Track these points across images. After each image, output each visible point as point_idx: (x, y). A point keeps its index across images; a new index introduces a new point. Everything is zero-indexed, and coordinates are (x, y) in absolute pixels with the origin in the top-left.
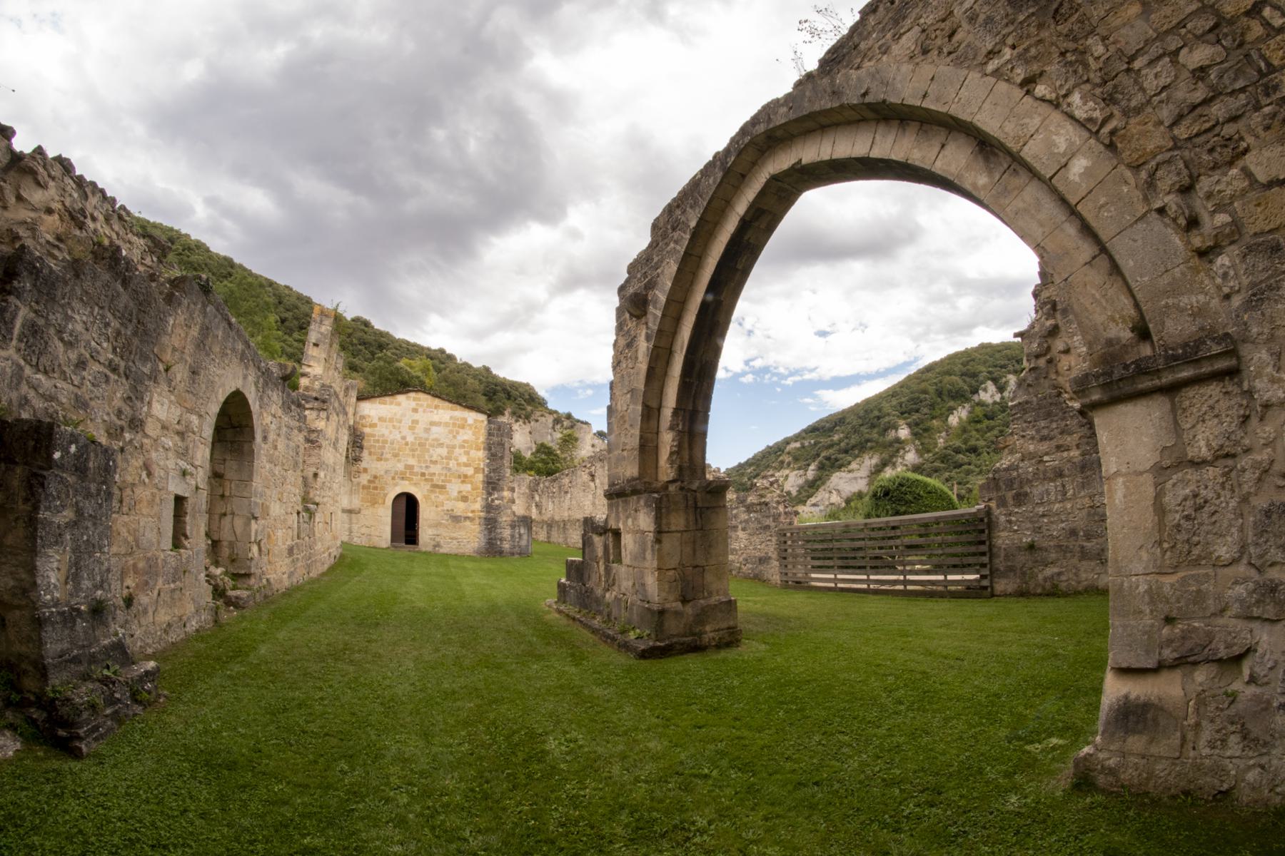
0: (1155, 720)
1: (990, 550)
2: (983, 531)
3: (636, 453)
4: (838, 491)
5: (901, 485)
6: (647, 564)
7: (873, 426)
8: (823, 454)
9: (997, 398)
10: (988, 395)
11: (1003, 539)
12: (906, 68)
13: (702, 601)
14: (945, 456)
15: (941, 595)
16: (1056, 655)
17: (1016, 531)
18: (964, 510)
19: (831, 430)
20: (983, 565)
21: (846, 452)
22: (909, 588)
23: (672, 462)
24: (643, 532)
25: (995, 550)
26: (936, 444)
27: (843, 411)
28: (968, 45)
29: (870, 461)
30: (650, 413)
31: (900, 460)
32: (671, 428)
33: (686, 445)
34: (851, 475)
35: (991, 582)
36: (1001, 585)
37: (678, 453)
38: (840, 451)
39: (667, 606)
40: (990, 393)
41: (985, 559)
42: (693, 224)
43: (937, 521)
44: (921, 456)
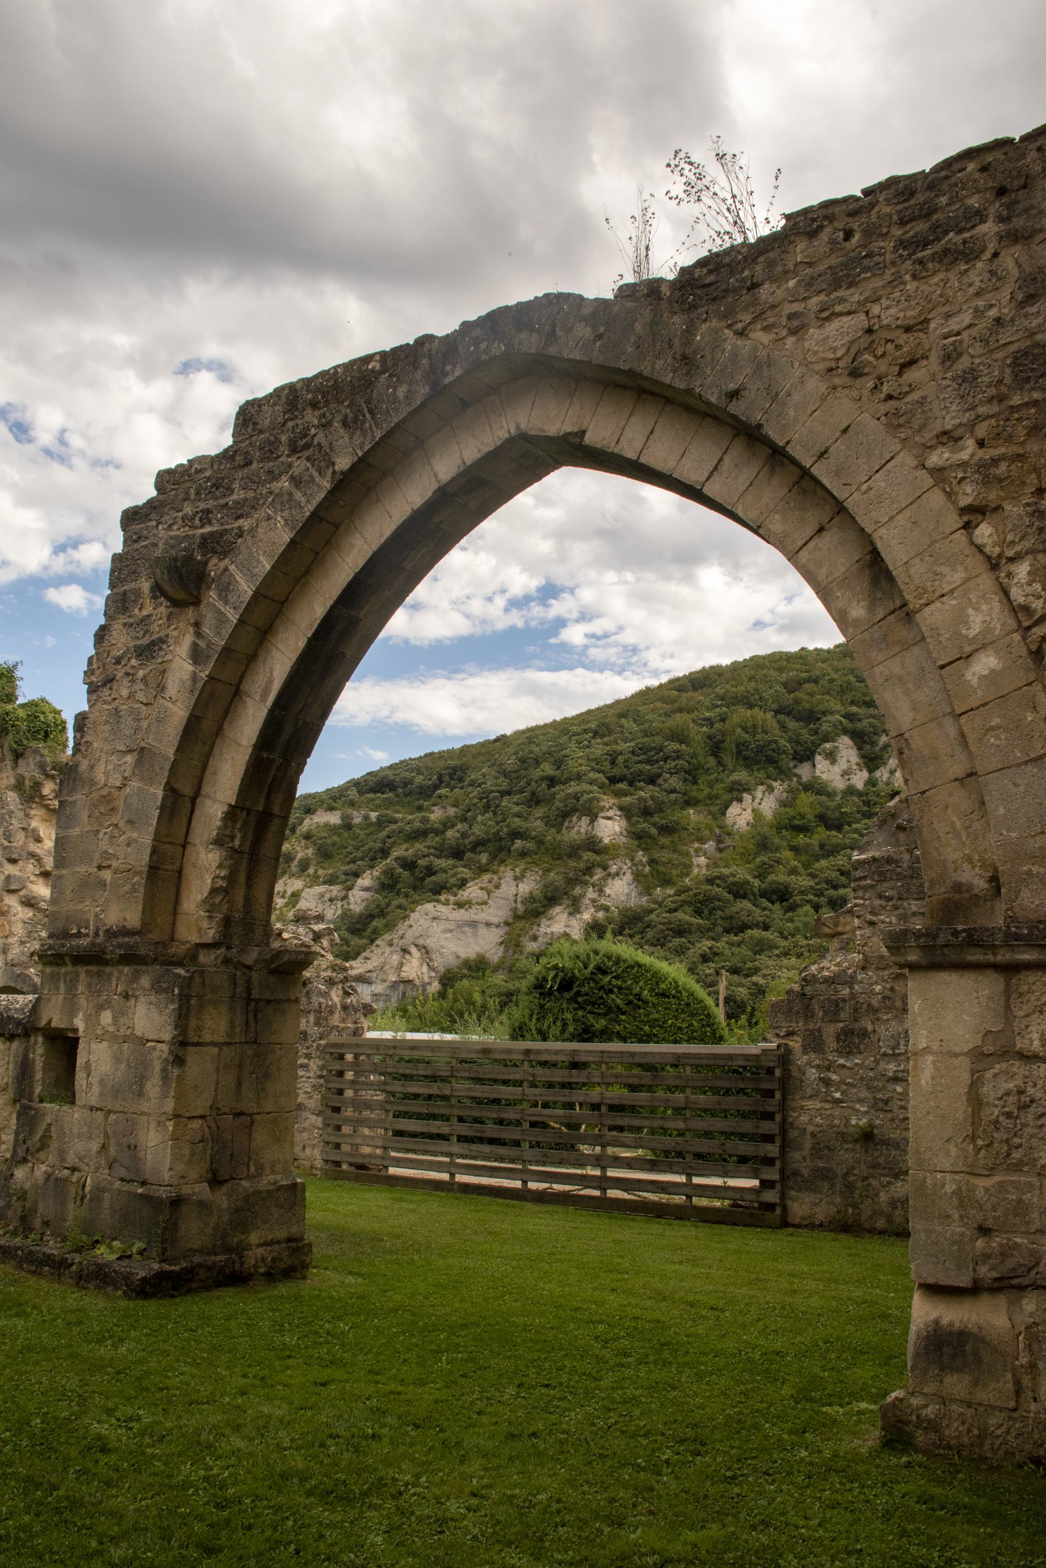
0: (976, 1354)
1: (784, 1132)
2: (770, 1094)
3: (139, 880)
4: (425, 950)
5: (601, 970)
6: (145, 1106)
7: (535, 800)
8: (397, 852)
9: (859, 780)
10: (837, 769)
11: (810, 1114)
12: (815, 385)
13: (245, 1184)
14: (709, 899)
15: (680, 1214)
16: (884, 1316)
17: (838, 1101)
18: (739, 1044)
19: (427, 792)
20: (769, 1161)
21: (457, 854)
22: (613, 1193)
23: (210, 905)
24: (143, 1041)
25: (793, 1134)
26: (688, 867)
27: (465, 750)
28: (922, 402)
29: (515, 886)
30: (179, 804)
31: (591, 894)
32: (218, 842)
33: (242, 878)
34: (461, 915)
35: (783, 1196)
36: (801, 1206)
37: (226, 891)
38: (441, 851)
39: (186, 1190)
40: (842, 765)
41: (772, 1150)
42: (343, 463)
43: (678, 1061)
44: (647, 891)
